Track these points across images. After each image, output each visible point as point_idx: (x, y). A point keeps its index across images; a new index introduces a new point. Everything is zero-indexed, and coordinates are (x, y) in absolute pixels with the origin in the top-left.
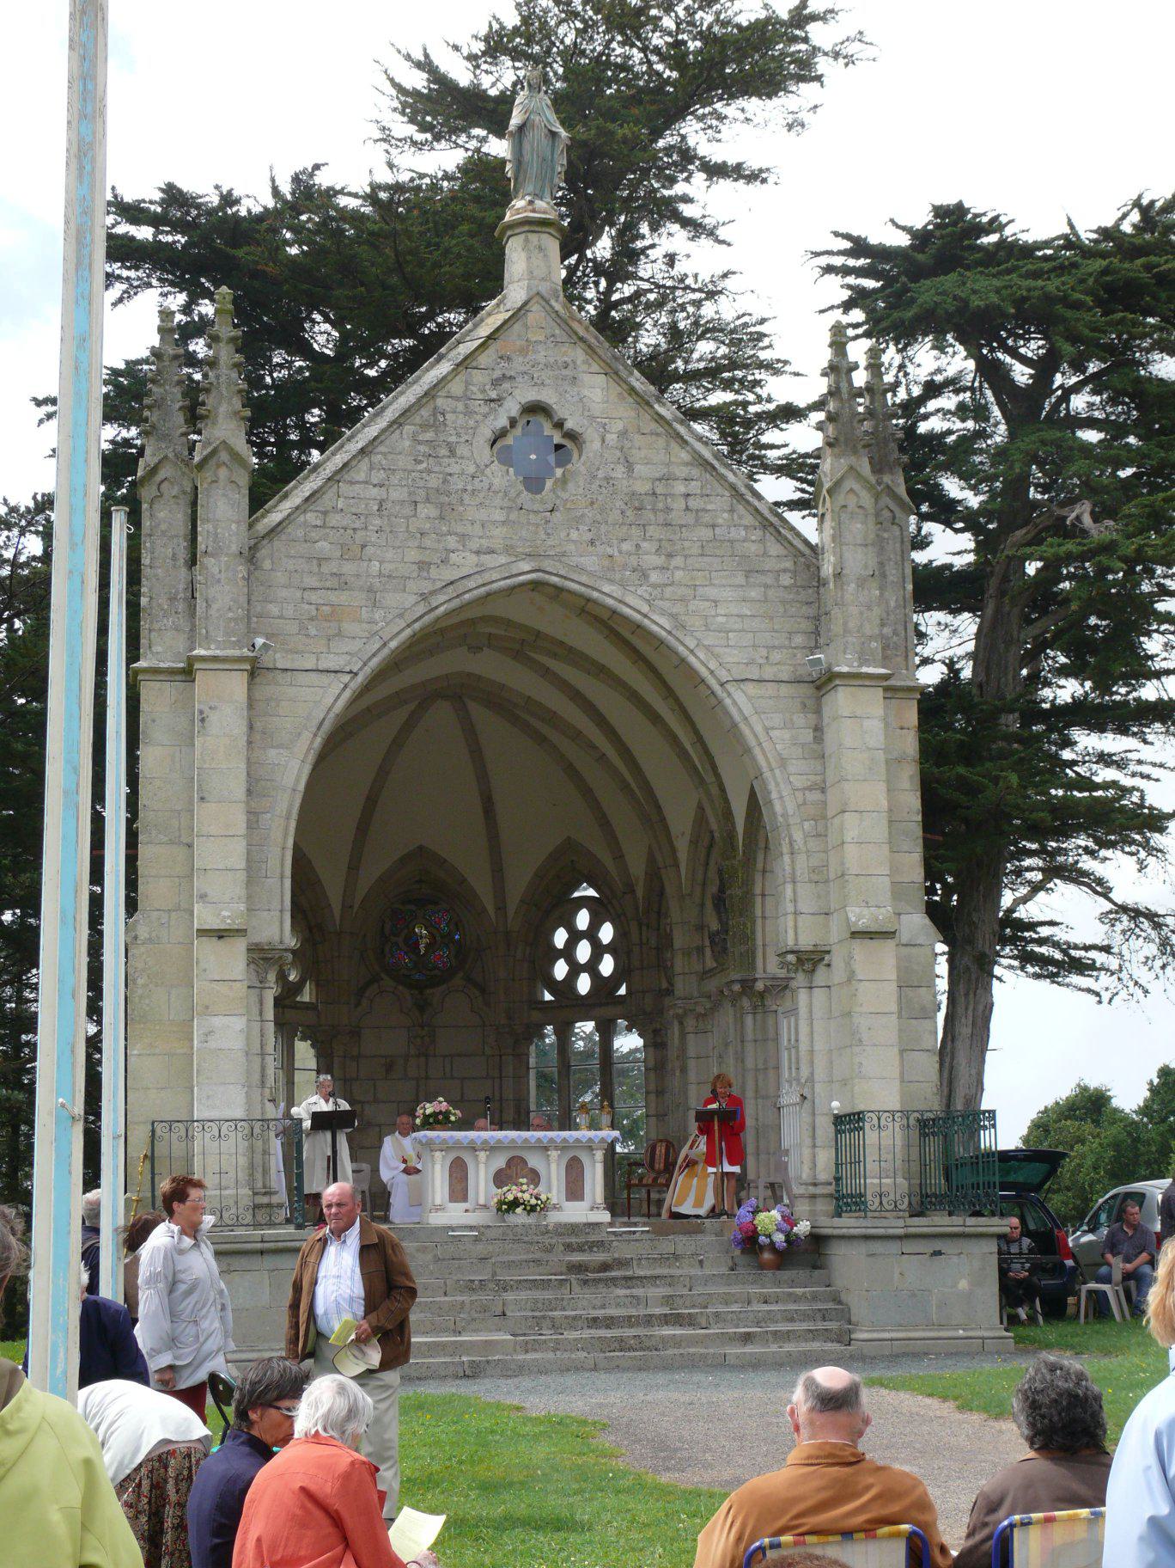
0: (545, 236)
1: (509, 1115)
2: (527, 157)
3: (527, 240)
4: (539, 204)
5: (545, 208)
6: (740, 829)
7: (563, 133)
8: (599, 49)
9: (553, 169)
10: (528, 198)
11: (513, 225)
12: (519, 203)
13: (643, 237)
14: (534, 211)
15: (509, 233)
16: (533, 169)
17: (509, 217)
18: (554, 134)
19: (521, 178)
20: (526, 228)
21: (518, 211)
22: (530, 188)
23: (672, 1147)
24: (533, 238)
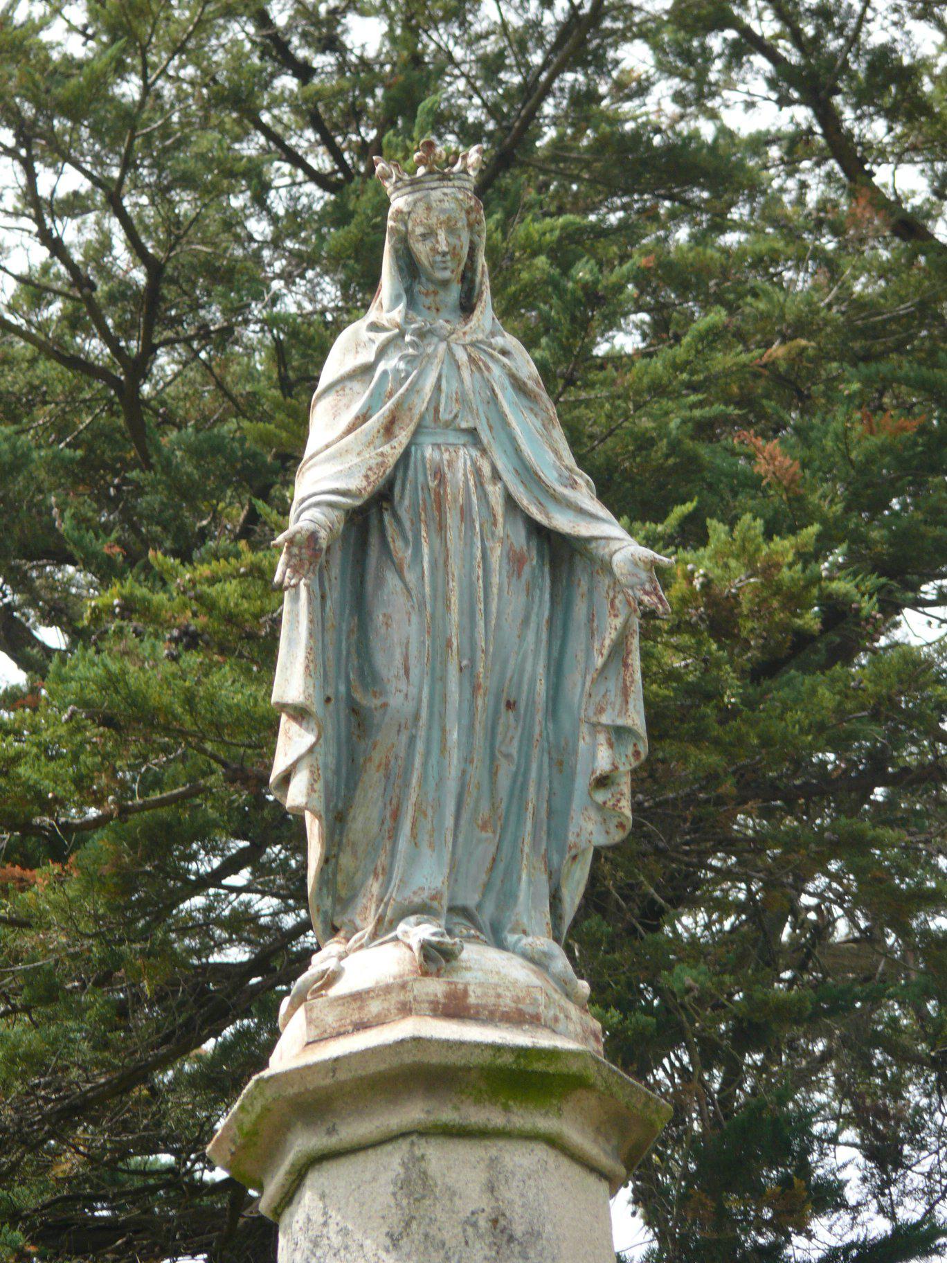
0: (522, 1159)
1: (634, 1068)
2: (401, 692)
3: (416, 1186)
4: (488, 967)
5: (527, 994)
6: (428, 599)
7: (624, 547)
8: (761, 467)
9: (561, 761)
10: (418, 932)
11: (319, 1098)
12: (364, 963)
13: (829, 1197)
14: (455, 1008)
15: (302, 1143)
16: (444, 762)
17: (297, 1046)
18: (560, 554)
19: (366, 817)
20: (413, 1113)
21: (360, 1010)
22: (429, 875)
23: (505, 234)
24: (459, 1170)
